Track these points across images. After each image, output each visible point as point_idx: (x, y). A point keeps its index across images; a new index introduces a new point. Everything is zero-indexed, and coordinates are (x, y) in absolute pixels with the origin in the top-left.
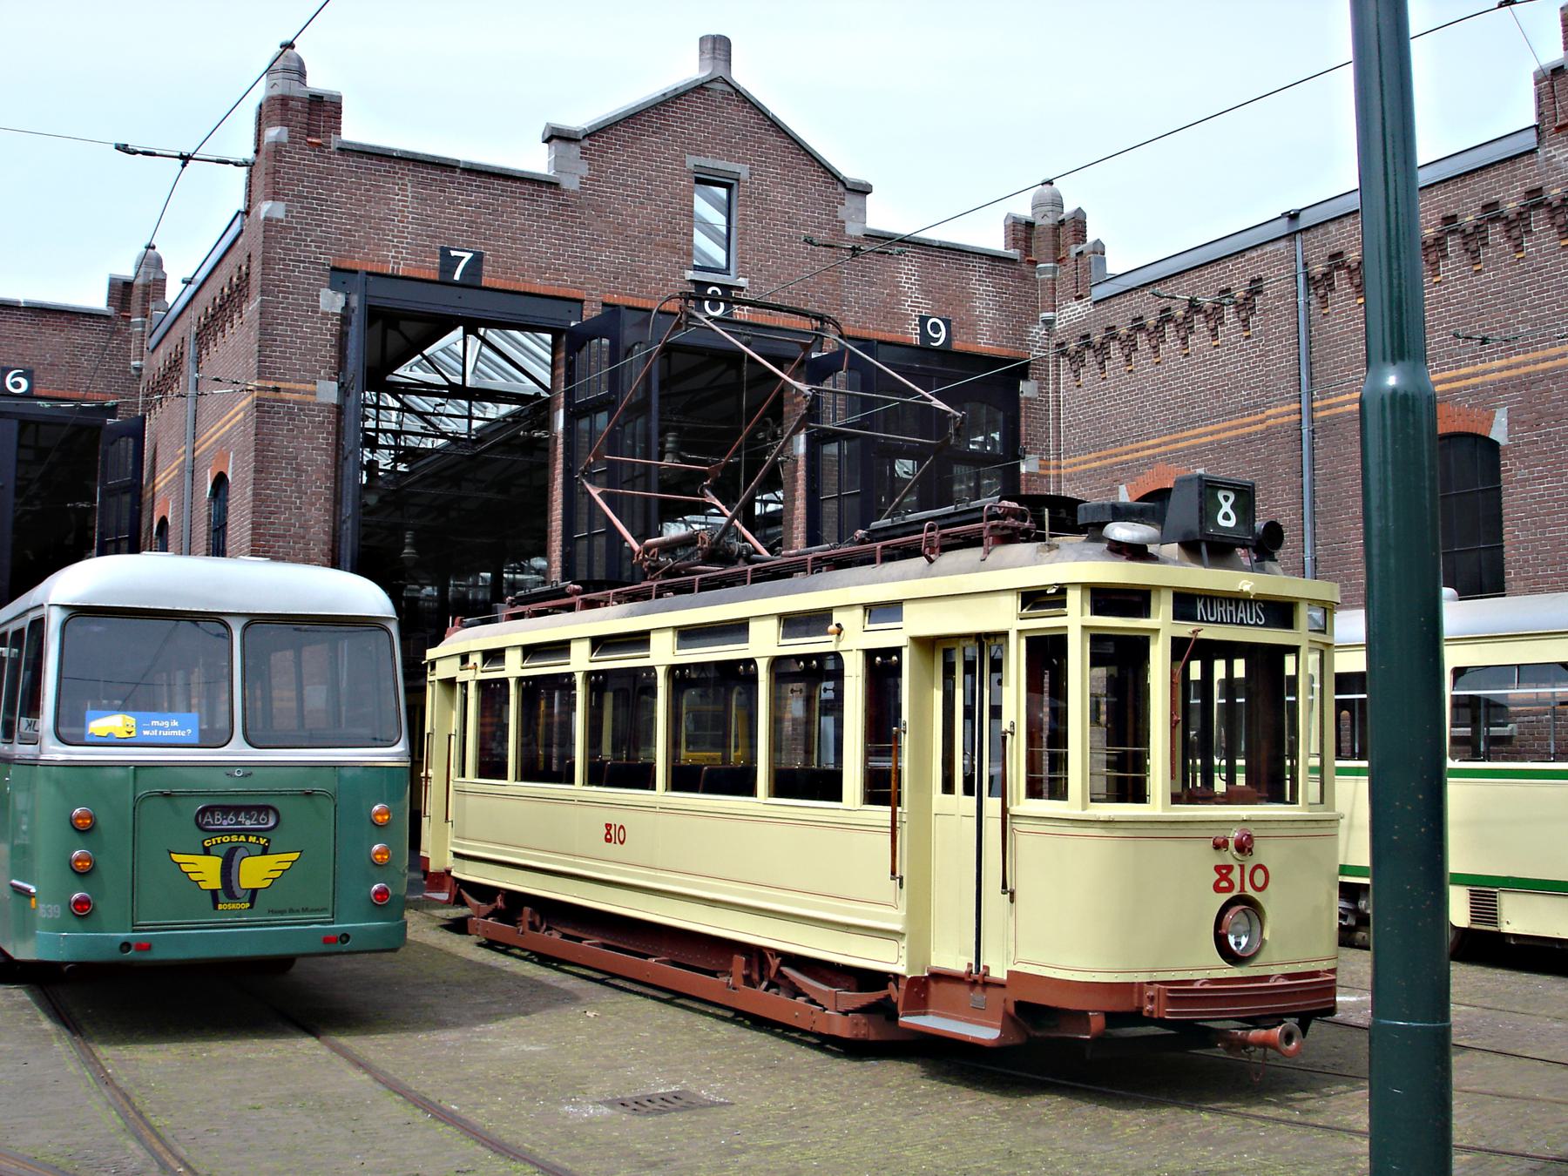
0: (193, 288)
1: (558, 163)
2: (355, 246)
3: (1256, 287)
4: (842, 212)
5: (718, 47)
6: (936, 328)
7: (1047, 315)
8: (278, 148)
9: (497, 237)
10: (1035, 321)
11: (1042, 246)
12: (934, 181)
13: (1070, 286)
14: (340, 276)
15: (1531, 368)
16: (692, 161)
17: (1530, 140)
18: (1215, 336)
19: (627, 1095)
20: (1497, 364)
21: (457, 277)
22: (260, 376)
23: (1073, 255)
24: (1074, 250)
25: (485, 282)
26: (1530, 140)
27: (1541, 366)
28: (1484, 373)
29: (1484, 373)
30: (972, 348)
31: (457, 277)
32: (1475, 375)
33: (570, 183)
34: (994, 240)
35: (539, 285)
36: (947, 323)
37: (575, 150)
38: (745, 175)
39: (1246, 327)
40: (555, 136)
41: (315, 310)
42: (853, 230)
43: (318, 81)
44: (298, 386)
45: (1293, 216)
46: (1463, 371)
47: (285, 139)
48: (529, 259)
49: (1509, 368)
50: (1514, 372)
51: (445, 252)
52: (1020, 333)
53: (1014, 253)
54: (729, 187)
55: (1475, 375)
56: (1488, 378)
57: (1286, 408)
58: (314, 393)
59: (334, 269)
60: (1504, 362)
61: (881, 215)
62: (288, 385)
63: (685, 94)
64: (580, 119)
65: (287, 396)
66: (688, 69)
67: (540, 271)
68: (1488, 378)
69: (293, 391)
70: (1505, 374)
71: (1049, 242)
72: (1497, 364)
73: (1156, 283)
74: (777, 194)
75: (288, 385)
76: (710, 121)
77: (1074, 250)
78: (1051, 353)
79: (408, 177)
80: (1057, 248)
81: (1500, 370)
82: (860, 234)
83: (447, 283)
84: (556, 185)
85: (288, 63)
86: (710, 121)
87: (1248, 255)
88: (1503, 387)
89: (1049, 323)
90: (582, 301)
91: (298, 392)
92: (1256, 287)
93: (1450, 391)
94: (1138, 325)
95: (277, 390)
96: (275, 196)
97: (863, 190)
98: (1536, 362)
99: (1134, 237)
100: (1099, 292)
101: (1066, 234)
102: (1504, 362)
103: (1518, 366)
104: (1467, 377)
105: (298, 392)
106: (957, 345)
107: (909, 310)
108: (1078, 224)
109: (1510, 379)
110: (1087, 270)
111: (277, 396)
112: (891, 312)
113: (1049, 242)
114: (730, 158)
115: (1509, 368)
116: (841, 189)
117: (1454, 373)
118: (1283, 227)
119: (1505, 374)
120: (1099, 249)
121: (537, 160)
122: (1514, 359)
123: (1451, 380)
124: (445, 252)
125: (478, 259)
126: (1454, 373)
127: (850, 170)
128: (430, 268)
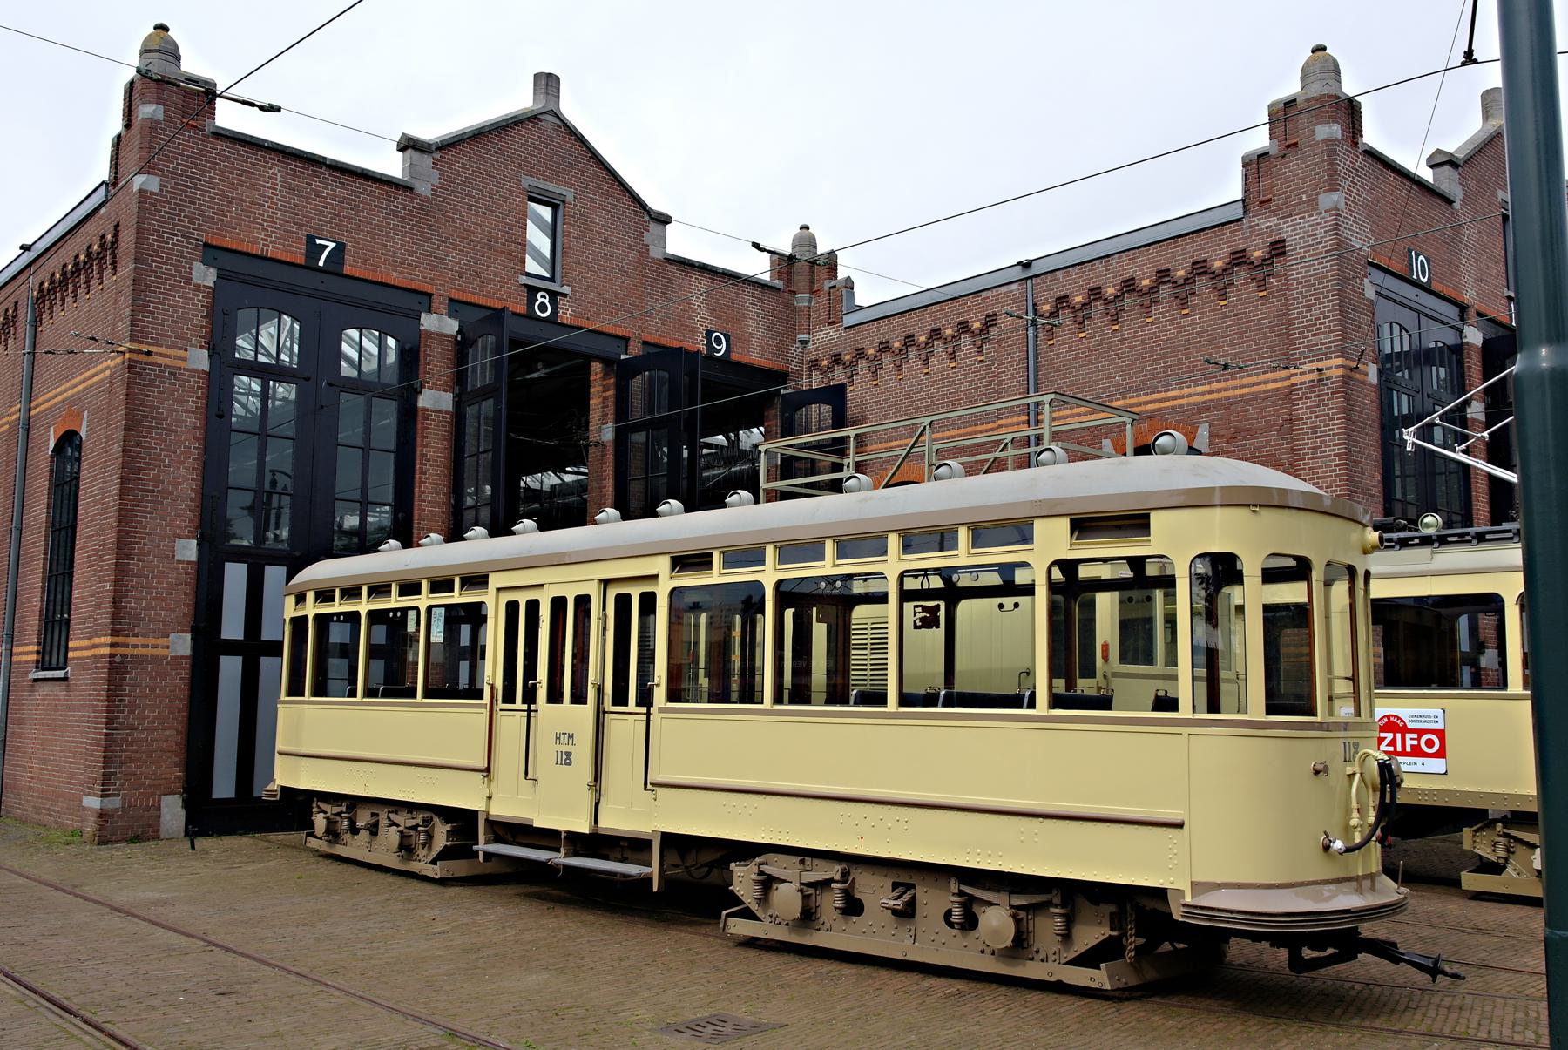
0: (28, 257)
1: (411, 168)
2: (228, 225)
3: (990, 321)
4: (647, 238)
5: (547, 83)
6: (718, 340)
7: (803, 336)
8: (152, 125)
9: (358, 231)
10: (794, 342)
11: (801, 279)
12: (719, 220)
13: (824, 313)
14: (211, 253)
15: (1230, 393)
16: (527, 181)
17: (1238, 212)
18: (953, 359)
19: (679, 1020)
20: (1200, 389)
21: (321, 263)
22: (132, 340)
23: (826, 288)
24: (827, 284)
25: (347, 270)
26: (1238, 212)
27: (1238, 392)
28: (1190, 395)
29: (1190, 395)
30: (746, 360)
31: (321, 263)
32: (1182, 397)
33: (423, 189)
34: (758, 267)
35: (394, 278)
36: (727, 337)
37: (427, 160)
38: (570, 198)
39: (981, 353)
40: (408, 145)
41: (188, 280)
42: (655, 253)
43: (193, 64)
44: (169, 351)
45: (1026, 265)
46: (1170, 394)
47: (161, 117)
48: (383, 256)
49: (1211, 392)
50: (1215, 396)
51: (311, 240)
52: (782, 349)
53: (778, 283)
54: (555, 207)
55: (1182, 397)
56: (1192, 400)
57: (1015, 419)
58: (185, 359)
59: (206, 245)
60: (1207, 388)
61: (678, 243)
62: (159, 350)
63: (521, 122)
64: (430, 132)
65: (159, 360)
66: (522, 100)
67: (396, 265)
68: (1192, 400)
69: (165, 356)
70: (1208, 397)
71: (806, 273)
72: (1200, 389)
73: (890, 315)
74: (594, 217)
75: (159, 350)
76: (535, 148)
77: (827, 284)
78: (805, 369)
79: (276, 170)
80: (812, 283)
81: (1203, 394)
82: (660, 257)
83: (311, 267)
84: (410, 189)
85: (161, 45)
86: (535, 148)
87: (984, 294)
88: (1206, 407)
89: (805, 343)
90: (430, 295)
91: (169, 356)
92: (990, 321)
93: (1160, 409)
94: (885, 347)
95: (149, 353)
96: (147, 168)
97: (664, 220)
98: (1235, 388)
99: (877, 281)
100: (849, 320)
101: (822, 272)
102: (1207, 388)
103: (1219, 391)
104: (1175, 398)
105: (169, 356)
106: (735, 357)
107: (695, 327)
108: (831, 261)
109: (1211, 401)
110: (839, 300)
111: (149, 359)
112: (684, 324)
113: (806, 273)
114: (558, 181)
115: (1211, 392)
116: (647, 218)
117: (1163, 395)
118: (1018, 273)
119: (1208, 397)
120: (849, 284)
121: (392, 164)
122: (1215, 386)
123: (1159, 401)
124: (311, 240)
125: (340, 249)
126: (1163, 395)
127: (655, 203)
128: (297, 254)
